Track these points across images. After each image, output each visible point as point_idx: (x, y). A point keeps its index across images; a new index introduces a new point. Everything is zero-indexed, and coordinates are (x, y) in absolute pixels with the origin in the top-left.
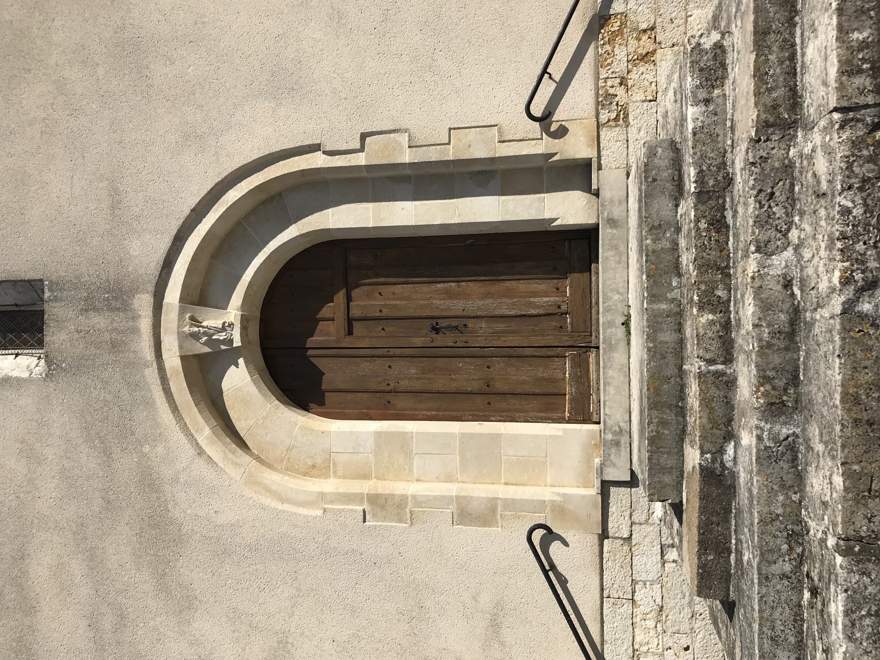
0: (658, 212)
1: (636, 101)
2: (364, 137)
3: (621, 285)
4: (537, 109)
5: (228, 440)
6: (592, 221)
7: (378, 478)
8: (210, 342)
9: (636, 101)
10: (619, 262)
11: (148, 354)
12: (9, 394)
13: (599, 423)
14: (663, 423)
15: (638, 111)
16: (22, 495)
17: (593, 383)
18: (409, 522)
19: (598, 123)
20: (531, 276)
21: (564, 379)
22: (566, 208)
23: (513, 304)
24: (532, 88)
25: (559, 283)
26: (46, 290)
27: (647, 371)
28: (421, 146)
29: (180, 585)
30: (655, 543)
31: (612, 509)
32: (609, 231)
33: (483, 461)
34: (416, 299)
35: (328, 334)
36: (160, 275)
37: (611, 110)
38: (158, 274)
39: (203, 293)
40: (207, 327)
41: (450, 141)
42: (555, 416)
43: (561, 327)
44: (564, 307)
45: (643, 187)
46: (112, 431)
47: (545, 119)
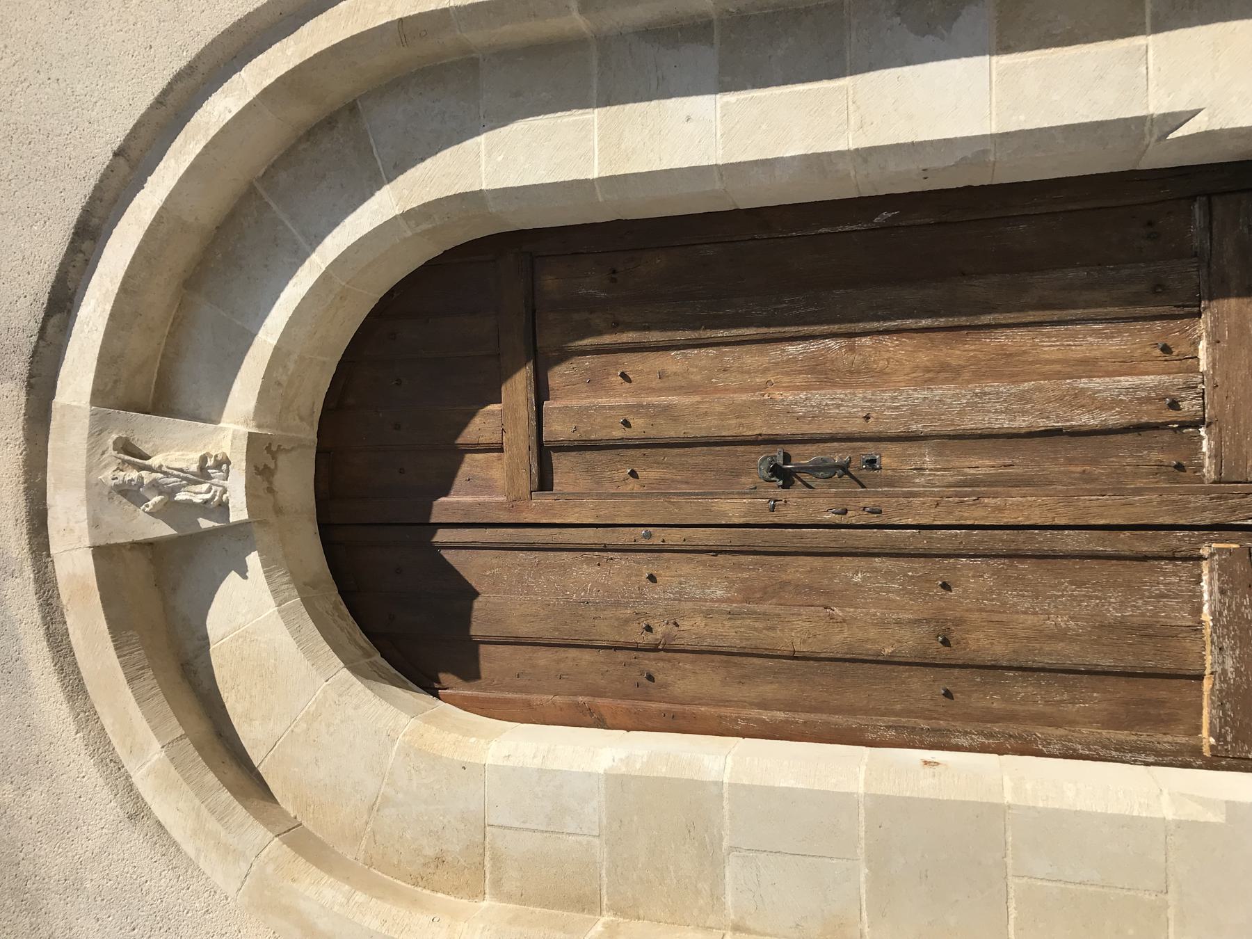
5: (211, 778)
7: (617, 911)
8: (170, 510)
20: (1080, 313)
21: (1197, 629)
23: (1022, 398)
25: (1172, 331)
34: (726, 390)
35: (488, 487)
36: (42, 330)
38: (35, 327)
39: (151, 384)
40: (159, 470)
42: (1166, 740)
43: (1179, 467)
44: (1189, 407)
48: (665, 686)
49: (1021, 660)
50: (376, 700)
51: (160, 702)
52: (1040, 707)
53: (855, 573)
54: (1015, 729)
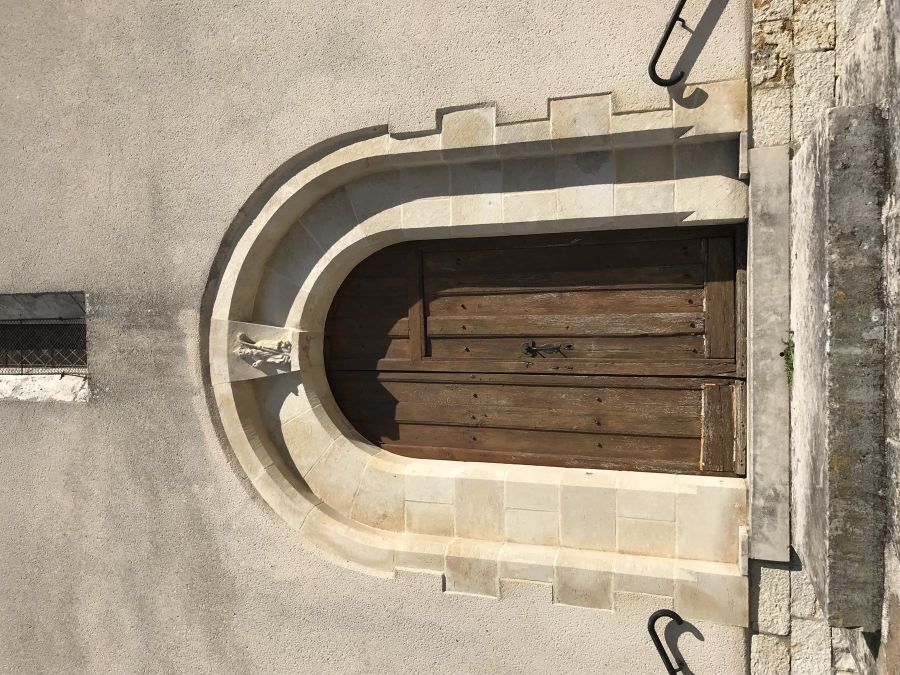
0: (850, 214)
1: (805, 52)
2: (440, 114)
3: (780, 302)
4: (665, 70)
5: (286, 482)
6: (738, 215)
7: (460, 534)
8: (264, 366)
9: (805, 52)
10: (777, 272)
11: (196, 379)
12: (53, 419)
13: (744, 476)
14: (853, 518)
15: (808, 65)
16: (69, 532)
17: (737, 425)
18: (498, 594)
19: (749, 84)
20: (656, 285)
21: (698, 418)
22: (703, 199)
23: (632, 321)
24: (658, 41)
25: (694, 294)
26: (87, 304)
27: (830, 443)
28: (512, 123)
29: (235, 647)
30: (823, 645)
31: (764, 596)
32: (763, 229)
33: (592, 520)
34: (507, 314)
35: (401, 354)
36: (207, 287)
37: (770, 67)
38: (203, 285)
39: (255, 310)
40: (260, 348)
41: (549, 115)
42: (686, 464)
43: (695, 351)
44: (699, 326)
45: (827, 178)
46: (159, 465)
47: (675, 83)
48: (481, 442)
49: (629, 431)
50: (356, 448)
51: (262, 449)
52: (637, 451)
53: (562, 394)
54: (627, 460)
